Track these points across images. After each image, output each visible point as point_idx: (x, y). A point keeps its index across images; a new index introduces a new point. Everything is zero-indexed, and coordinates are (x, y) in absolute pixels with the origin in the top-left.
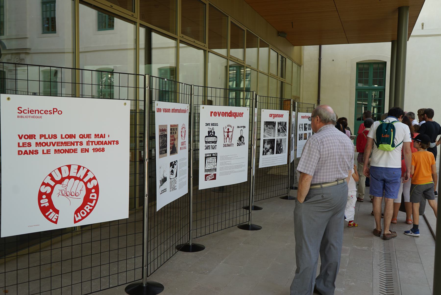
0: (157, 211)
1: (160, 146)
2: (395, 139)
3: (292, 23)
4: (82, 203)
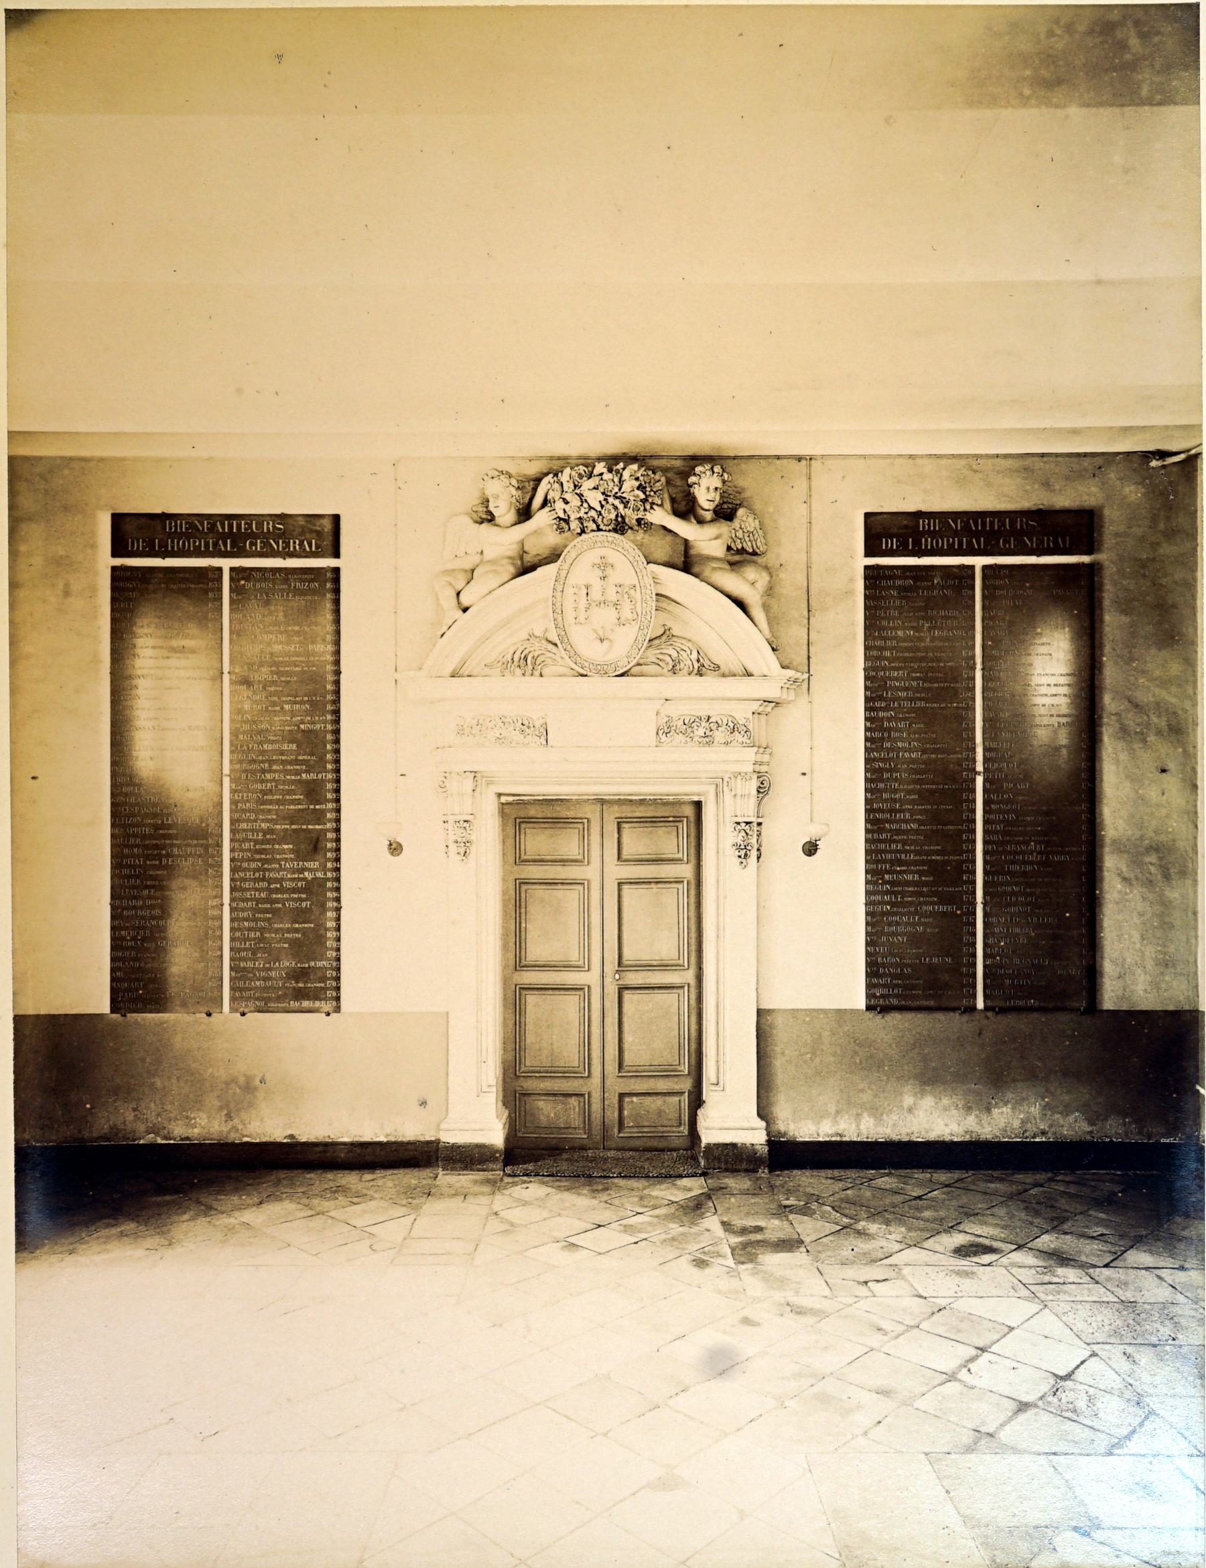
2: (816, 1319)
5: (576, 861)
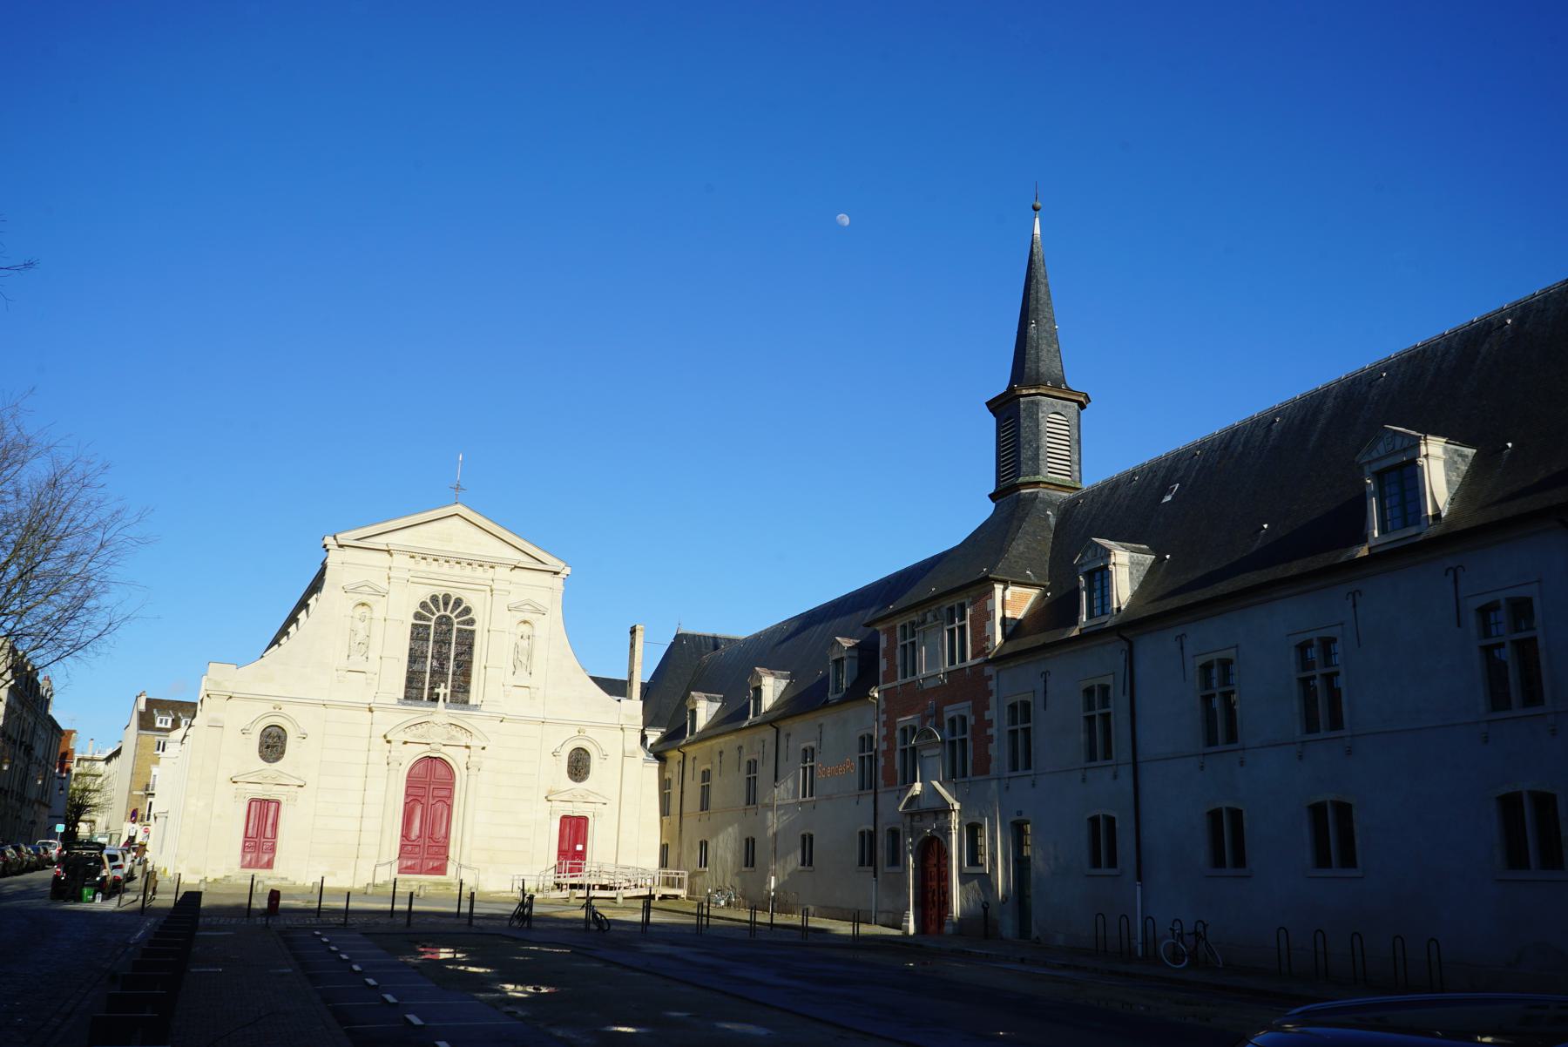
0: (1071, 635)
1: (178, 899)
3: (763, 741)
4: (991, 513)
5: (1118, 876)
